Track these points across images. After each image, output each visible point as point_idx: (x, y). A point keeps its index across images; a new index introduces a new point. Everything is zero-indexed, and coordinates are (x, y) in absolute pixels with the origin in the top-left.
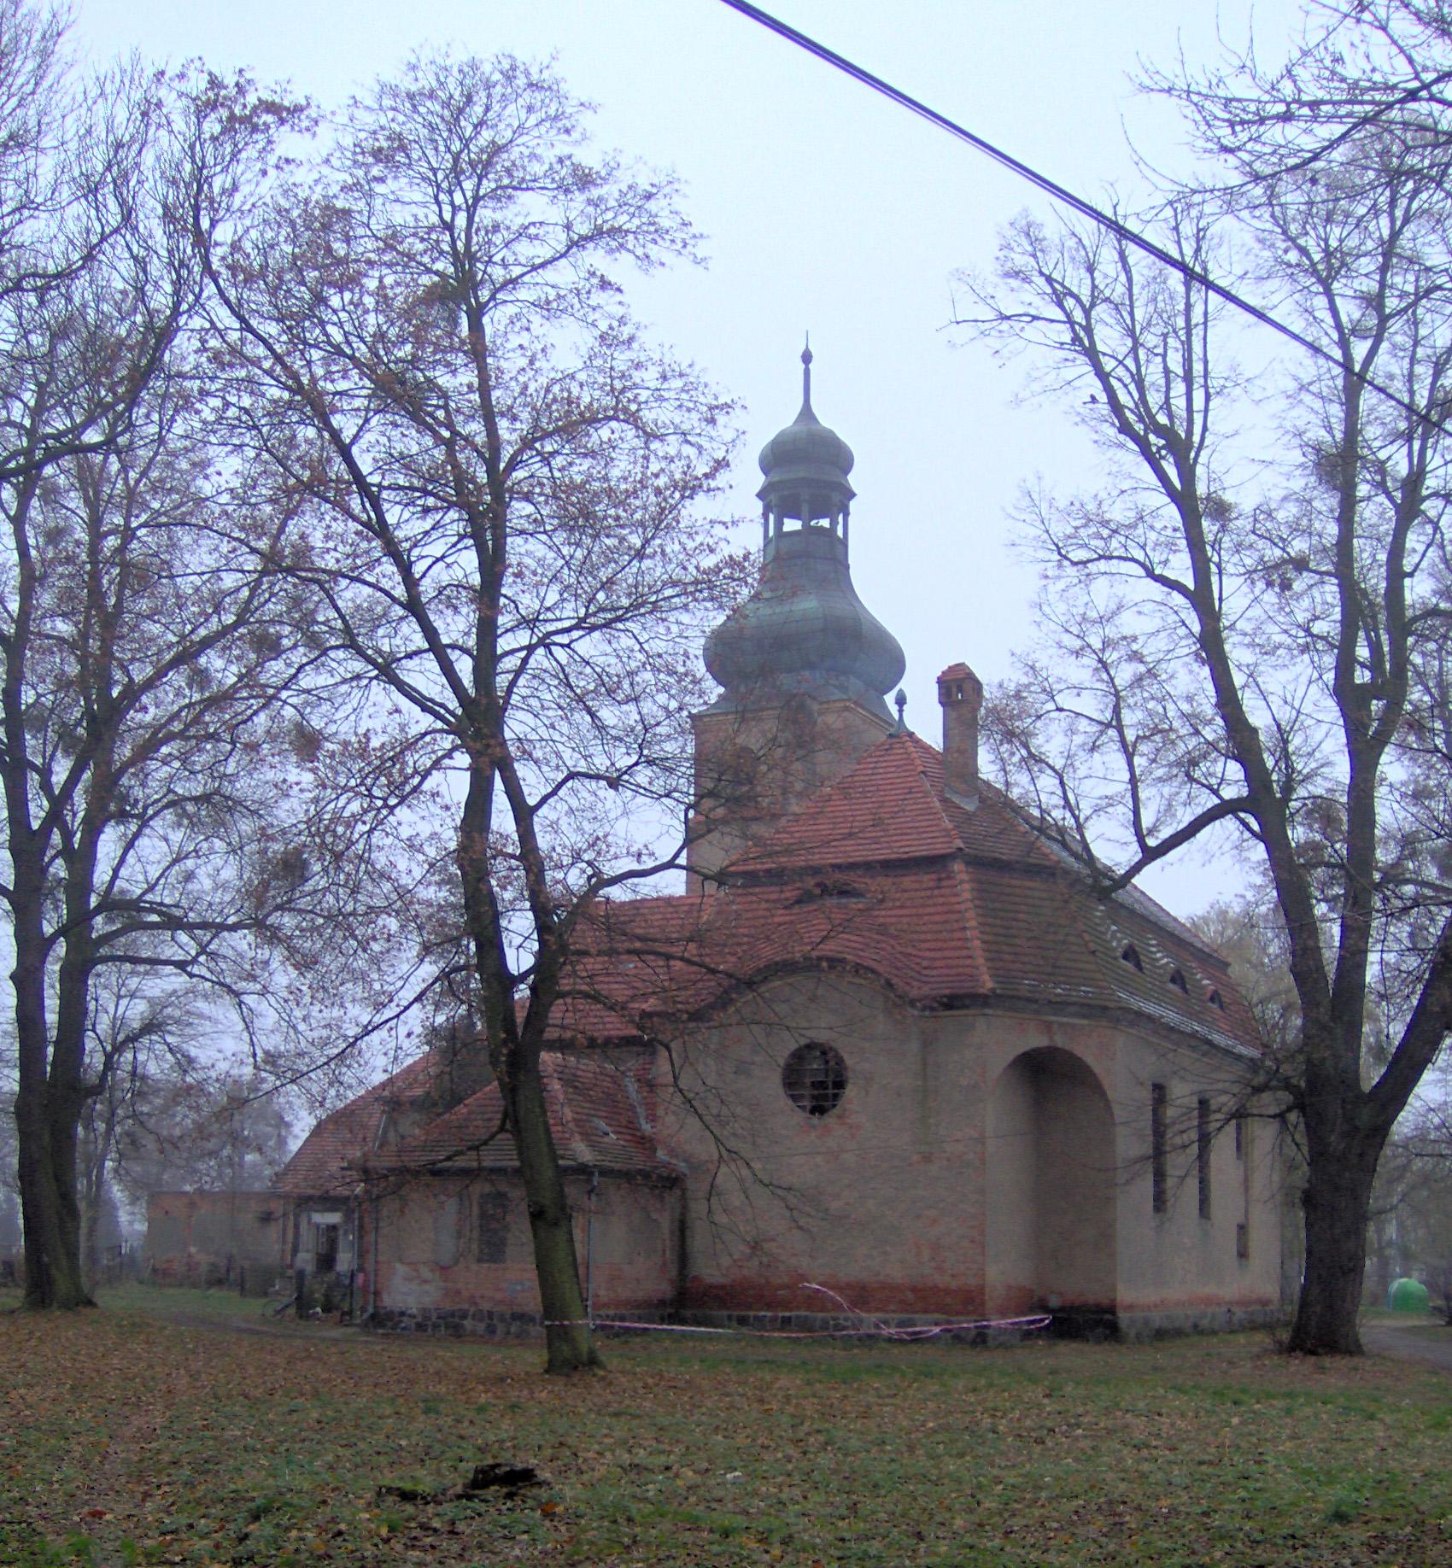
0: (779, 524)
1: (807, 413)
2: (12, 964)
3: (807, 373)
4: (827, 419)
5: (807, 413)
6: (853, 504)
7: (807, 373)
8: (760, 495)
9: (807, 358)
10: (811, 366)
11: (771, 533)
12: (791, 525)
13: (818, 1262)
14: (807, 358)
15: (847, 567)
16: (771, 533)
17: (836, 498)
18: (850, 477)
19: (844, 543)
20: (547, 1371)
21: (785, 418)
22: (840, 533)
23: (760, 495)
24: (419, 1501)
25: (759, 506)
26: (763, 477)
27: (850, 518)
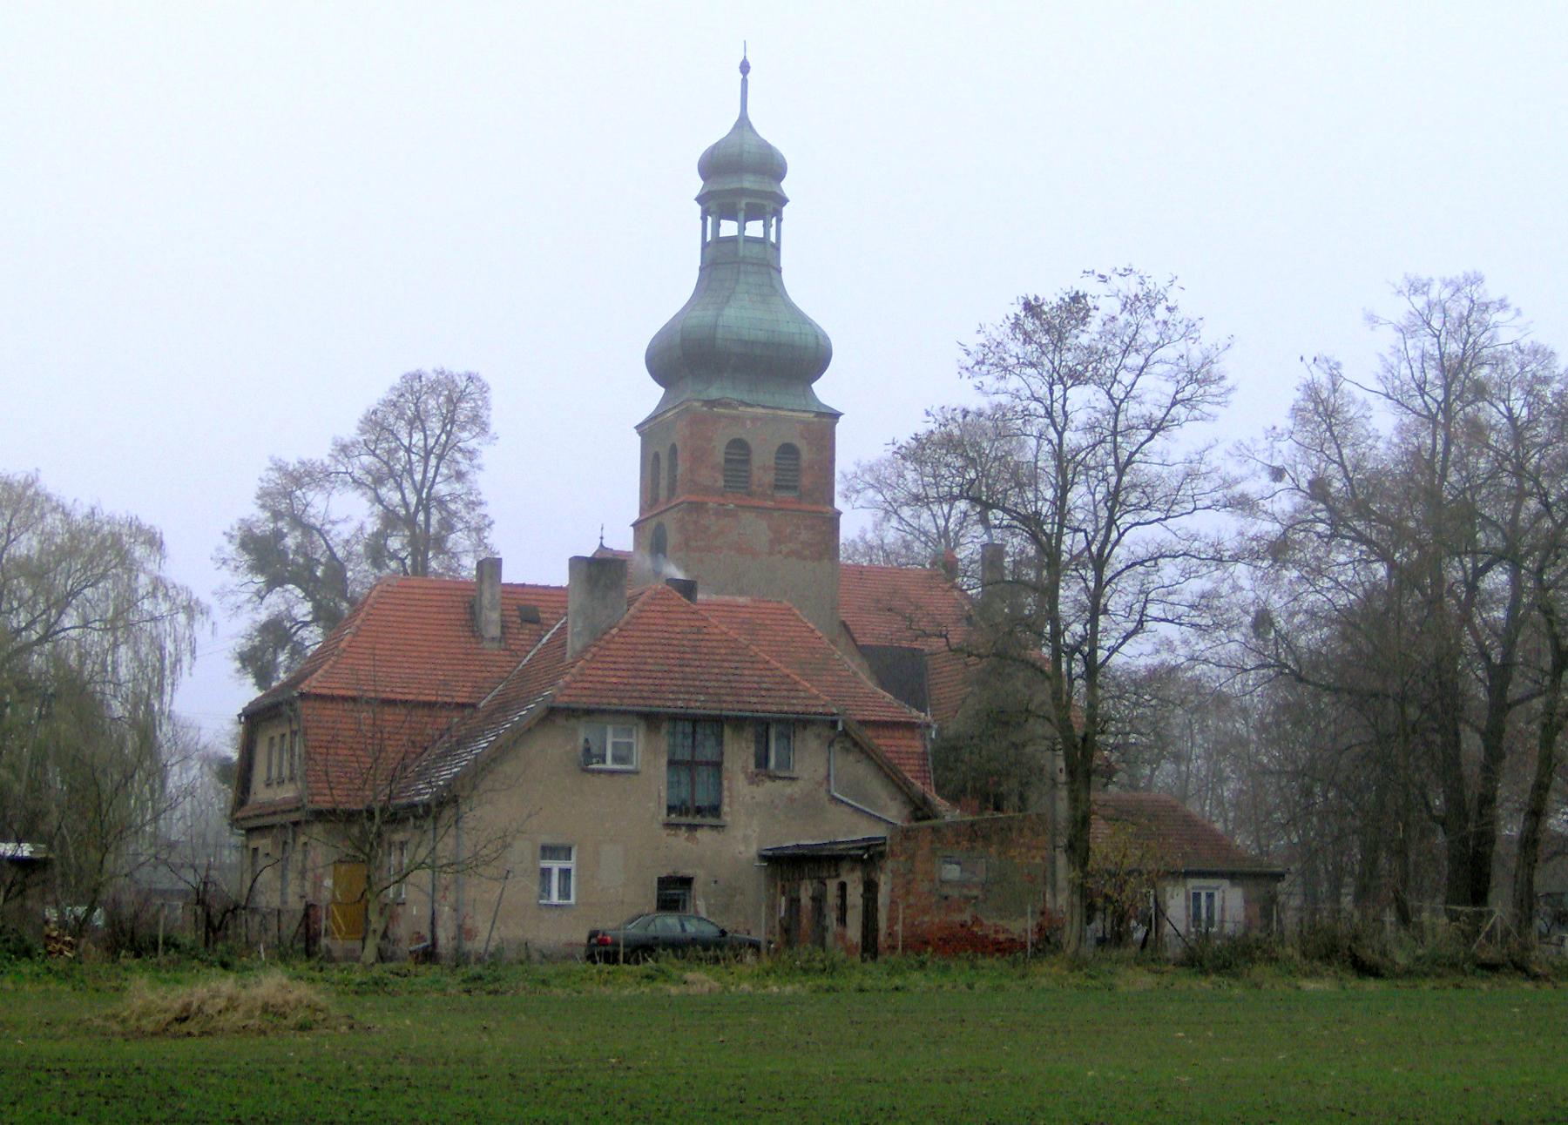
0: (717, 226)
1: (743, 122)
2: (636, 516)
3: (745, 82)
4: (770, 129)
5: (743, 122)
6: (785, 210)
7: (745, 82)
8: (699, 199)
9: (745, 68)
10: (749, 76)
11: (709, 238)
12: (729, 228)
13: (197, 626)
14: (745, 68)
15: (779, 271)
16: (709, 238)
17: (770, 205)
18: (784, 184)
19: (777, 247)
20: (882, 855)
21: (718, 129)
22: (773, 239)
23: (699, 199)
24: (286, 709)
25: (698, 208)
26: (701, 183)
27: (783, 225)
